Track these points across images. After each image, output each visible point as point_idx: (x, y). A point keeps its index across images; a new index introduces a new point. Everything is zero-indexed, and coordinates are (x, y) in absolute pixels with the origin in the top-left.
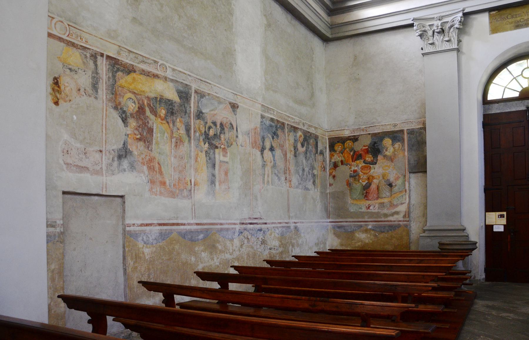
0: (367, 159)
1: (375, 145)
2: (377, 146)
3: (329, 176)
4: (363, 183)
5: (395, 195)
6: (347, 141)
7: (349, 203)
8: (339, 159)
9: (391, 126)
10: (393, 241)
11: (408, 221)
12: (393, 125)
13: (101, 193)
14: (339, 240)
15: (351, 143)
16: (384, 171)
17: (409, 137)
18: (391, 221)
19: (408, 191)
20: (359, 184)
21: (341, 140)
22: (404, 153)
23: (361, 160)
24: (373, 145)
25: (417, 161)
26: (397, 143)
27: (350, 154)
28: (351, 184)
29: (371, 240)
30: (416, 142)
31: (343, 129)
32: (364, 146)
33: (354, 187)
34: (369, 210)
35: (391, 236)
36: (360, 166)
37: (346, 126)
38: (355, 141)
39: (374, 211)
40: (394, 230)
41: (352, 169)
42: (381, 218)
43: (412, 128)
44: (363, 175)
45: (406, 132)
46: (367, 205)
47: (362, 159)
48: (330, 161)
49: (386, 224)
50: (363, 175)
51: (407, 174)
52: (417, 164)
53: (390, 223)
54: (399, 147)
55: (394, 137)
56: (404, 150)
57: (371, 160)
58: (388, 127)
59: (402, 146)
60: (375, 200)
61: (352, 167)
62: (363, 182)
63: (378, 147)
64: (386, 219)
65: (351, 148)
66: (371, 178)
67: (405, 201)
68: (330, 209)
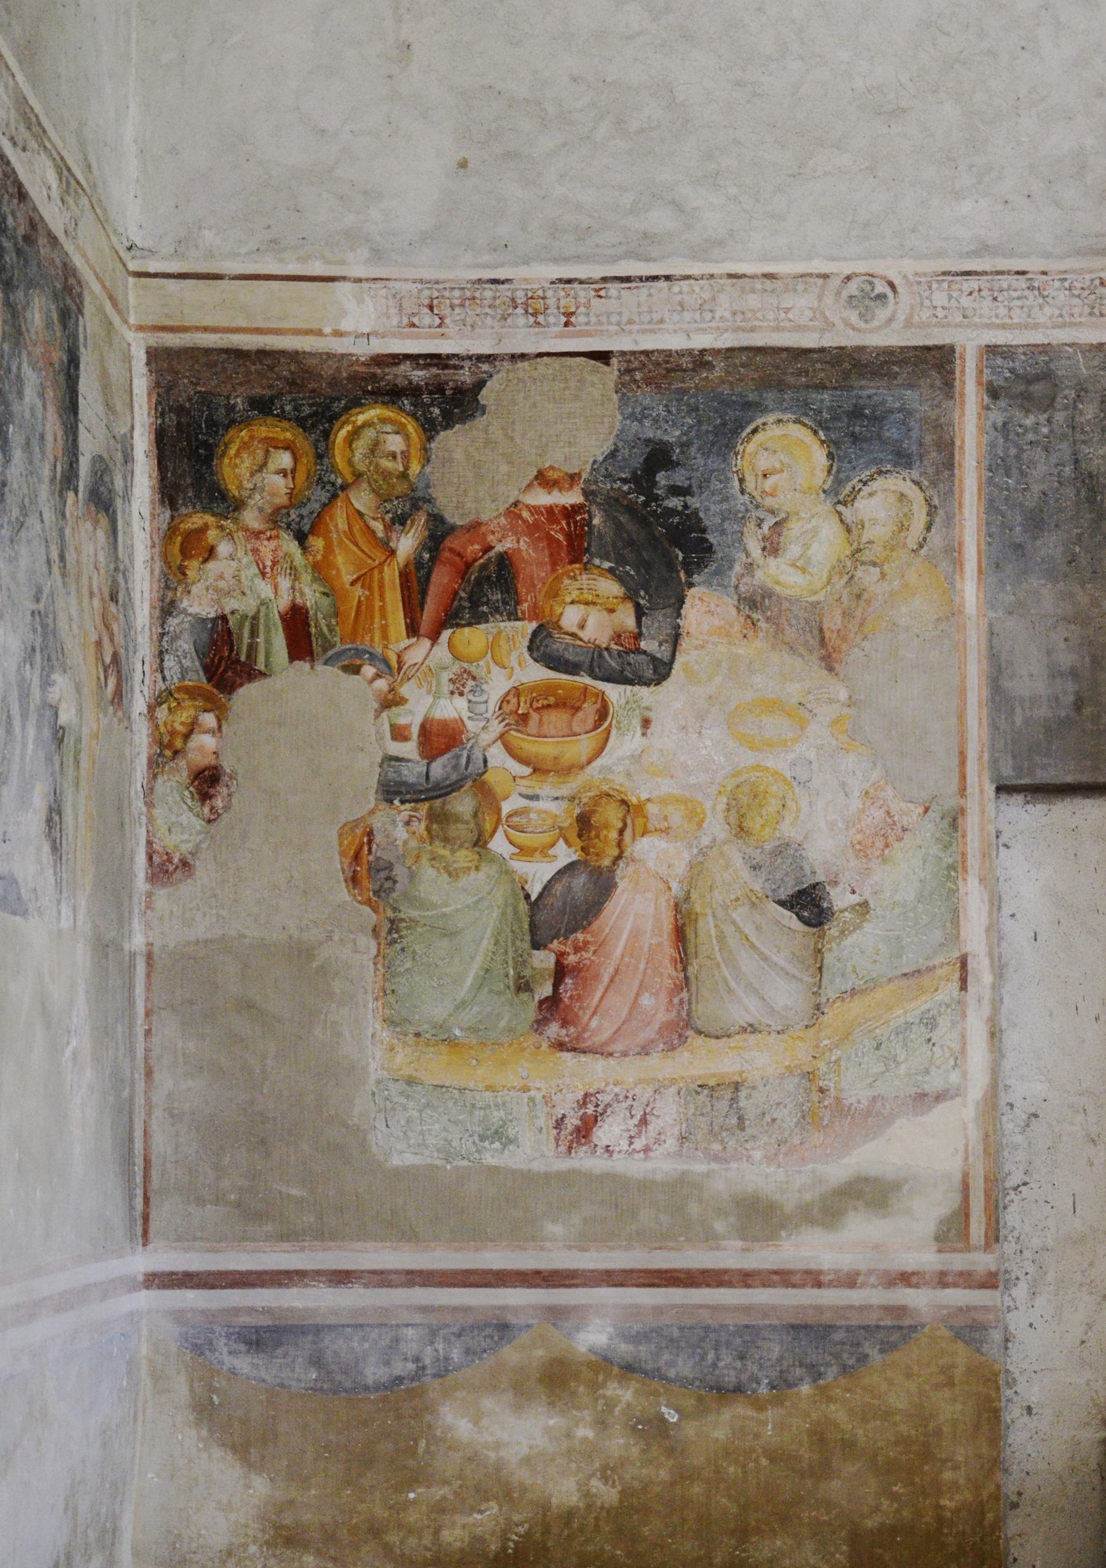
0: (570, 617)
1: (662, 478)
2: (676, 491)
3: (155, 766)
4: (521, 867)
5: (855, 1008)
6: (356, 403)
7: (374, 1070)
8: (265, 589)
9: (829, 300)
10: (835, 1488)
11: (990, 1281)
12: (853, 288)
13: (234, 325)
14: (261, 1485)
15: (400, 430)
16: (747, 758)
17: (1004, 428)
18: (814, 1279)
19: (987, 978)
20: (479, 879)
21: (292, 383)
22: (950, 588)
23: (507, 626)
24: (634, 479)
25: (1074, 673)
26: (879, 483)
27: (393, 553)
28: (399, 872)
29: (606, 1473)
30: (1070, 492)
31: (317, 268)
32: (543, 480)
33: (423, 905)
34: (585, 1161)
35: (820, 1436)
36: (498, 685)
37: (353, 237)
38: (448, 422)
39: (634, 1167)
40: (844, 1370)
41: (412, 716)
42: (711, 1239)
43: (1037, 338)
44: (524, 786)
45: (971, 365)
46: (567, 1105)
47: (513, 616)
48: (167, 609)
49: (766, 1311)
50: (524, 786)
51: (972, 805)
52: (1079, 704)
53: (806, 1297)
54: (903, 527)
55: (856, 413)
56: (953, 552)
57: (617, 637)
58: (801, 304)
59: (932, 511)
60: (645, 1051)
61: (405, 690)
62: (525, 852)
63: (694, 502)
64: (763, 1258)
65: (401, 488)
66: (612, 815)
67: (954, 1077)
68: (161, 1142)
